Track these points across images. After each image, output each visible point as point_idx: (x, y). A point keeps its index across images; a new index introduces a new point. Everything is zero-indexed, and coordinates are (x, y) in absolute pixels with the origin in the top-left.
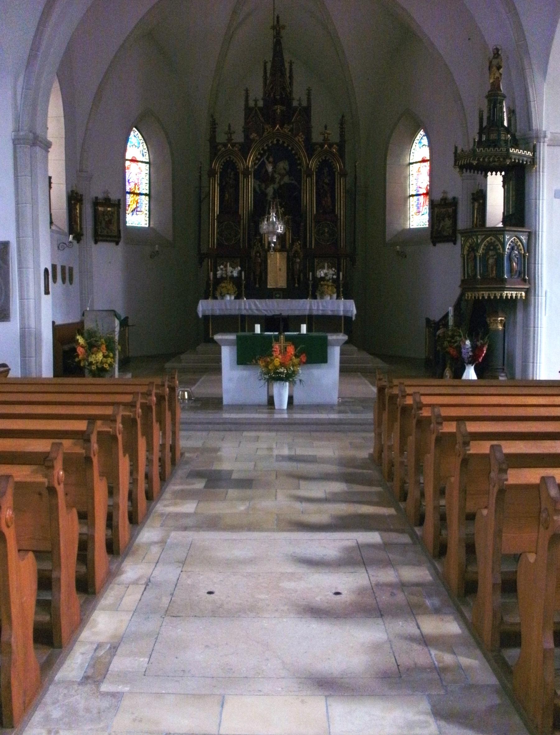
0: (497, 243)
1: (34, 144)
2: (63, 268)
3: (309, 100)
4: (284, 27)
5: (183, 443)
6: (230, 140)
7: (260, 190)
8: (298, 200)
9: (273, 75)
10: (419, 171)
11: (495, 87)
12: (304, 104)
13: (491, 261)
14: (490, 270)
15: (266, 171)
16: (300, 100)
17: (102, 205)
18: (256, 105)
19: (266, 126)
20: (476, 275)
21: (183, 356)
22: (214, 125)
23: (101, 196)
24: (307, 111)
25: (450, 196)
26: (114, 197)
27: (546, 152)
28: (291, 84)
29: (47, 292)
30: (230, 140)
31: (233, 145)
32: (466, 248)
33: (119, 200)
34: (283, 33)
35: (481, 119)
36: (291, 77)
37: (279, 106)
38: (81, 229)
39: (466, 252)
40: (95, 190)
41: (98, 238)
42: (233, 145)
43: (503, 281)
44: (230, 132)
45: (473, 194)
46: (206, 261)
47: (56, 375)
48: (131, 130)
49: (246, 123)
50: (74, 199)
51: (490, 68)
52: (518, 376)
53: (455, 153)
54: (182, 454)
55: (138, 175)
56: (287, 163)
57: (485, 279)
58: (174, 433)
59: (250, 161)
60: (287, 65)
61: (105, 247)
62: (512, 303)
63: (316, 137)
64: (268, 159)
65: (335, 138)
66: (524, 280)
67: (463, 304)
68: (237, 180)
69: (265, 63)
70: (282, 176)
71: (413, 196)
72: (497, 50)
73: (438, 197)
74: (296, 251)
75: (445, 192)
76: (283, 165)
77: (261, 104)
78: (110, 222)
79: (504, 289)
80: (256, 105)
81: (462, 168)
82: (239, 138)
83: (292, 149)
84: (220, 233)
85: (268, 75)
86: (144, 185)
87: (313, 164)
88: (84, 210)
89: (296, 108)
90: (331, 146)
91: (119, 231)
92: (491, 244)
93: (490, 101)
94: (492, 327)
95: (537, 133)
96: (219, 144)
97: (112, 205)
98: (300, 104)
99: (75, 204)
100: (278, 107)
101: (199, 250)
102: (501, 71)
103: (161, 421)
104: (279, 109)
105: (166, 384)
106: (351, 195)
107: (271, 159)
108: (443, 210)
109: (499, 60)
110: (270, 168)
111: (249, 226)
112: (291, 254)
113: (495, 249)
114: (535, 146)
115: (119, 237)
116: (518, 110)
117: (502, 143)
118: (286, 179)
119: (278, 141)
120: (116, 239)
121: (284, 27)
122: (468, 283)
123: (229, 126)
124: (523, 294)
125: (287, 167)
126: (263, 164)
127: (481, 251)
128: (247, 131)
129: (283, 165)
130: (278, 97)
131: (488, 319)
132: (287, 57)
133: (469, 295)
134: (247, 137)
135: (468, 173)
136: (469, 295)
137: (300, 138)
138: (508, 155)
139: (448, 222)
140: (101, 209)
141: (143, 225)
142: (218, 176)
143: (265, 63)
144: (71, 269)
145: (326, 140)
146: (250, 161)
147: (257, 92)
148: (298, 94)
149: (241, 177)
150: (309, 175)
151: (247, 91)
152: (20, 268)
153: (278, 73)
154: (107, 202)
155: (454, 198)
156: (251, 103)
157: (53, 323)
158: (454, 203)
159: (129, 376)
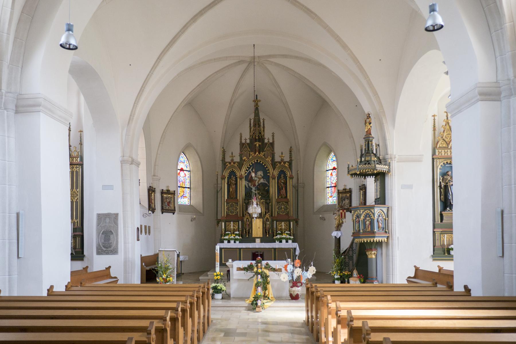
0: (370, 213)
1: (132, 164)
2: (145, 227)
3: (273, 139)
4: (260, 101)
5: (212, 316)
6: (232, 160)
7: (249, 186)
8: (268, 192)
9: (255, 125)
10: (332, 174)
11: (369, 133)
12: (271, 141)
13: (368, 223)
14: (367, 227)
15: (251, 176)
16: (268, 139)
17: (165, 193)
18: (246, 142)
19: (251, 153)
20: (360, 230)
21: (209, 273)
22: (224, 152)
23: (165, 189)
24: (272, 145)
25: (348, 188)
26: (172, 189)
27: (395, 166)
28: (264, 131)
29: (138, 240)
30: (232, 160)
31: (234, 163)
32: (355, 216)
33: (174, 191)
34: (259, 104)
35: (362, 150)
36: (264, 127)
37: (257, 143)
38: (155, 206)
39: (354, 218)
40: (161, 186)
41: (163, 211)
42: (234, 163)
43: (374, 233)
44: (232, 156)
45: (360, 187)
46: (220, 223)
47: (141, 283)
48: (180, 154)
49: (241, 151)
50: (151, 190)
51: (366, 123)
52: (384, 282)
53: (348, 168)
54: (212, 321)
55: (184, 178)
56: (262, 172)
57: (364, 232)
58: (208, 310)
59: (243, 172)
60: (262, 121)
61: (168, 216)
62: (380, 244)
63: (277, 159)
64: (252, 170)
65: (287, 159)
66: (386, 232)
67: (354, 245)
68: (236, 181)
69: (250, 120)
70: (260, 179)
71: (328, 187)
72: (369, 114)
73: (341, 188)
74: (267, 218)
75: (345, 186)
76: (260, 173)
77: (248, 141)
78: (169, 202)
79: (374, 237)
80: (246, 142)
81: (352, 175)
82: (237, 159)
83: (265, 165)
84: (228, 209)
85: (252, 126)
86: (187, 183)
87: (276, 173)
88: (156, 196)
89: (266, 144)
90: (285, 163)
91: (175, 207)
92: (367, 214)
93: (366, 141)
94: (369, 257)
95: (391, 155)
96: (227, 162)
97: (172, 194)
98: (268, 141)
99: (152, 193)
100: (257, 143)
101: (217, 217)
102: (371, 125)
103: (203, 304)
104: (257, 144)
105: (206, 287)
106: (296, 188)
107: (254, 170)
108: (344, 195)
109: (370, 119)
110: (253, 175)
111: (243, 205)
112: (265, 220)
113: (370, 216)
114: (389, 163)
115: (175, 210)
116: (380, 145)
117: (373, 162)
118: (262, 181)
119: (257, 160)
120: (173, 211)
121: (260, 101)
122: (356, 234)
123: (232, 153)
124: (386, 239)
125: (262, 175)
126: (250, 173)
127: (362, 218)
128: (241, 156)
129: (260, 173)
130: (257, 138)
131: (367, 253)
132: (262, 116)
133: (356, 240)
134: (241, 159)
135: (355, 178)
136: (356, 240)
137: (269, 159)
138: (375, 168)
139: (347, 201)
140: (165, 195)
141: (187, 204)
142: (226, 180)
143: (250, 120)
144: (149, 227)
145: (282, 160)
146: (243, 172)
147: (247, 136)
148: (268, 136)
149: (238, 180)
150: (274, 178)
151: (241, 134)
152: (124, 227)
153: (257, 124)
154: (168, 192)
155: (350, 189)
156: (243, 141)
157: (141, 255)
158: (350, 191)
159: (181, 283)
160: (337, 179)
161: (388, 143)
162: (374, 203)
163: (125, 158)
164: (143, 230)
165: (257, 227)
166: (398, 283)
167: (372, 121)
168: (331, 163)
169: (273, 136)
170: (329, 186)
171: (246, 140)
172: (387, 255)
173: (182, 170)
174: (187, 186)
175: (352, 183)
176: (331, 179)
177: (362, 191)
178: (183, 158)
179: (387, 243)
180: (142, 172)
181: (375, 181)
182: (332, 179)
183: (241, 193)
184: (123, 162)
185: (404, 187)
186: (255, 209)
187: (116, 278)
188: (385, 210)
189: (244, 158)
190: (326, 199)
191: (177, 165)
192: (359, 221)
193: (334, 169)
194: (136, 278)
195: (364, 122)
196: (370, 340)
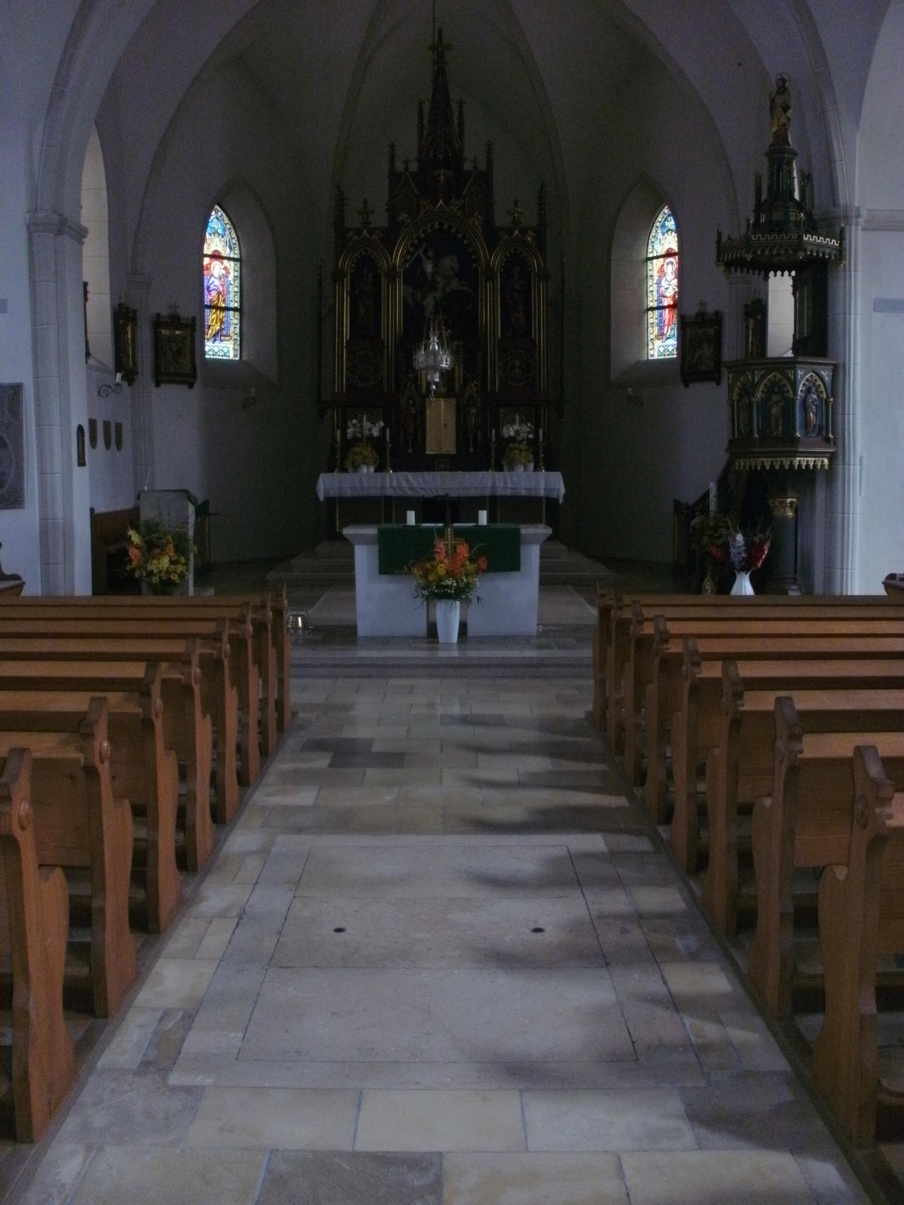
1: (60, 232)
2: (107, 425)
3: (489, 160)
6: (366, 223)
11: (780, 138)
12: (482, 166)
13: (775, 410)
15: (424, 272)
17: (167, 325)
18: (406, 169)
20: (751, 432)
22: (340, 199)
23: (164, 312)
24: (486, 177)
25: (710, 309)
26: (185, 313)
27: (859, 241)
28: (461, 136)
29: (82, 463)
30: (366, 223)
31: (371, 232)
32: (736, 389)
33: (194, 319)
36: (461, 125)
39: (735, 397)
42: (371, 232)
43: (794, 441)
45: (746, 306)
48: (211, 209)
50: (123, 317)
51: (772, 108)
52: (818, 589)
53: (719, 242)
54: (294, 714)
55: (222, 276)
60: (455, 107)
61: (173, 393)
62: (807, 477)
63: (501, 219)
65: (530, 219)
66: (827, 440)
72: (783, 81)
73: (692, 310)
75: (702, 304)
76: (450, 263)
77: (414, 167)
79: (795, 454)
80: (406, 169)
81: (728, 265)
82: (380, 220)
83: (464, 237)
85: (425, 122)
86: (231, 296)
87: (496, 261)
90: (523, 232)
91: (194, 367)
92: (774, 383)
93: (771, 161)
94: (778, 513)
97: (183, 327)
98: (475, 167)
99: (126, 325)
100: (442, 171)
103: (261, 663)
104: (442, 175)
105: (269, 604)
107: (430, 254)
110: (429, 268)
113: (781, 391)
114: (842, 231)
115: (194, 376)
116: (815, 174)
118: (454, 285)
120: (189, 379)
122: (739, 445)
123: (365, 202)
125: (456, 266)
126: (418, 260)
129: (450, 263)
130: (441, 157)
131: (771, 502)
133: (741, 464)
134: (392, 218)
135: (739, 274)
136: (741, 464)
137: (476, 221)
138: (800, 245)
139: (707, 350)
140: (164, 332)
141: (231, 357)
142: (347, 280)
143: (421, 103)
144: (119, 427)
147: (409, 149)
148: (473, 151)
149: (384, 280)
150: (491, 278)
151: (392, 146)
154: (175, 321)
155: (717, 313)
156: (400, 167)
157: (92, 510)
158: (717, 320)
159: (211, 592)
160: (680, 285)
161: (840, 167)
162: (790, 354)
163: (40, 215)
164: (102, 434)
165: (440, 425)
166: (856, 592)
167: (793, 103)
168: (660, 236)
169: (489, 152)
170: (655, 304)
171: (406, 162)
172: (830, 510)
173: (216, 256)
174: (232, 305)
175: (721, 294)
176: (659, 283)
177: (752, 322)
178: (217, 221)
179: (830, 475)
180: (95, 262)
181: (796, 287)
182: (664, 283)
183: (393, 318)
184: (33, 228)
185: (884, 306)
186: (437, 357)
187: (15, 577)
188: (826, 374)
189: (403, 216)
190: (641, 341)
191: (203, 240)
192: (750, 405)
193: (669, 254)
194: (80, 580)
195: (768, 103)
196: (890, 823)
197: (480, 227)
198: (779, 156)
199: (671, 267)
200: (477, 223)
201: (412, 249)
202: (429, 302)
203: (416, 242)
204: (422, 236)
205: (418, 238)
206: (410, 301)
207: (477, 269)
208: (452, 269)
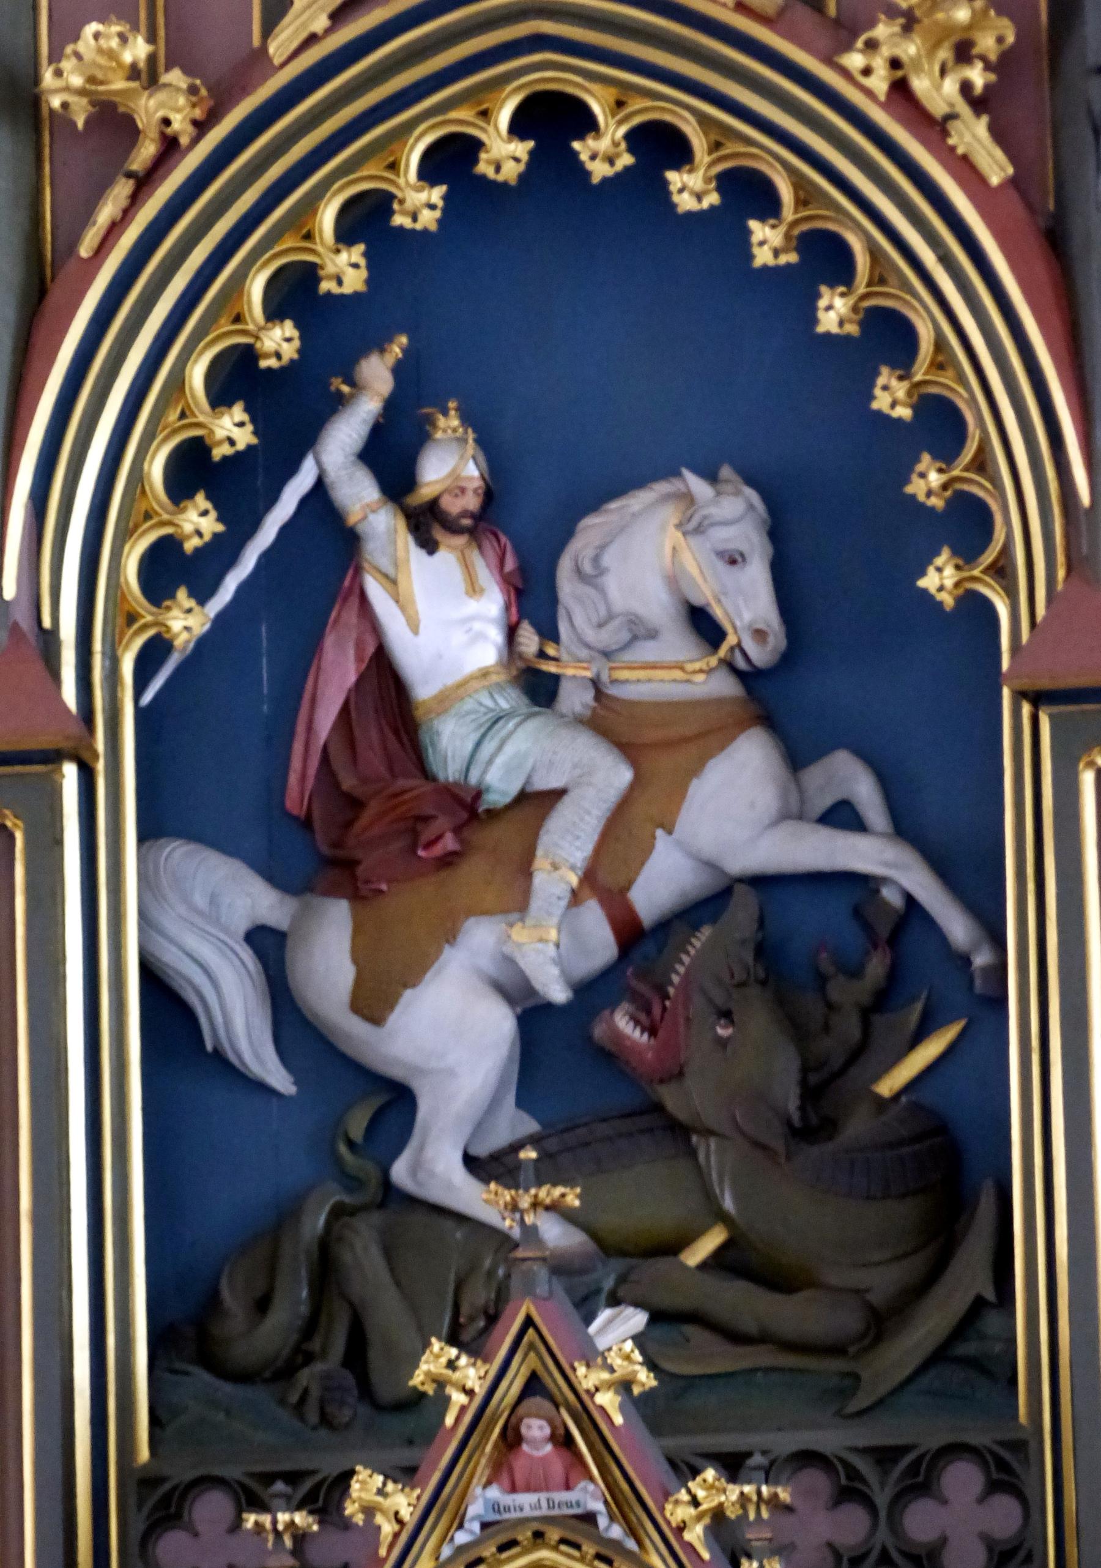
76: (676, 556)
107: (449, 466)
110: (443, 620)
118: (735, 813)
125: (749, 605)
197: (973, 135)
198: (477, 678)
199: (278, 1564)
200: (938, 91)
201: (232, 430)
202: (452, 1038)
203: (280, 342)
204: (346, 270)
205: (295, 292)
206: (236, 1013)
207: (976, 611)
208: (703, 625)
